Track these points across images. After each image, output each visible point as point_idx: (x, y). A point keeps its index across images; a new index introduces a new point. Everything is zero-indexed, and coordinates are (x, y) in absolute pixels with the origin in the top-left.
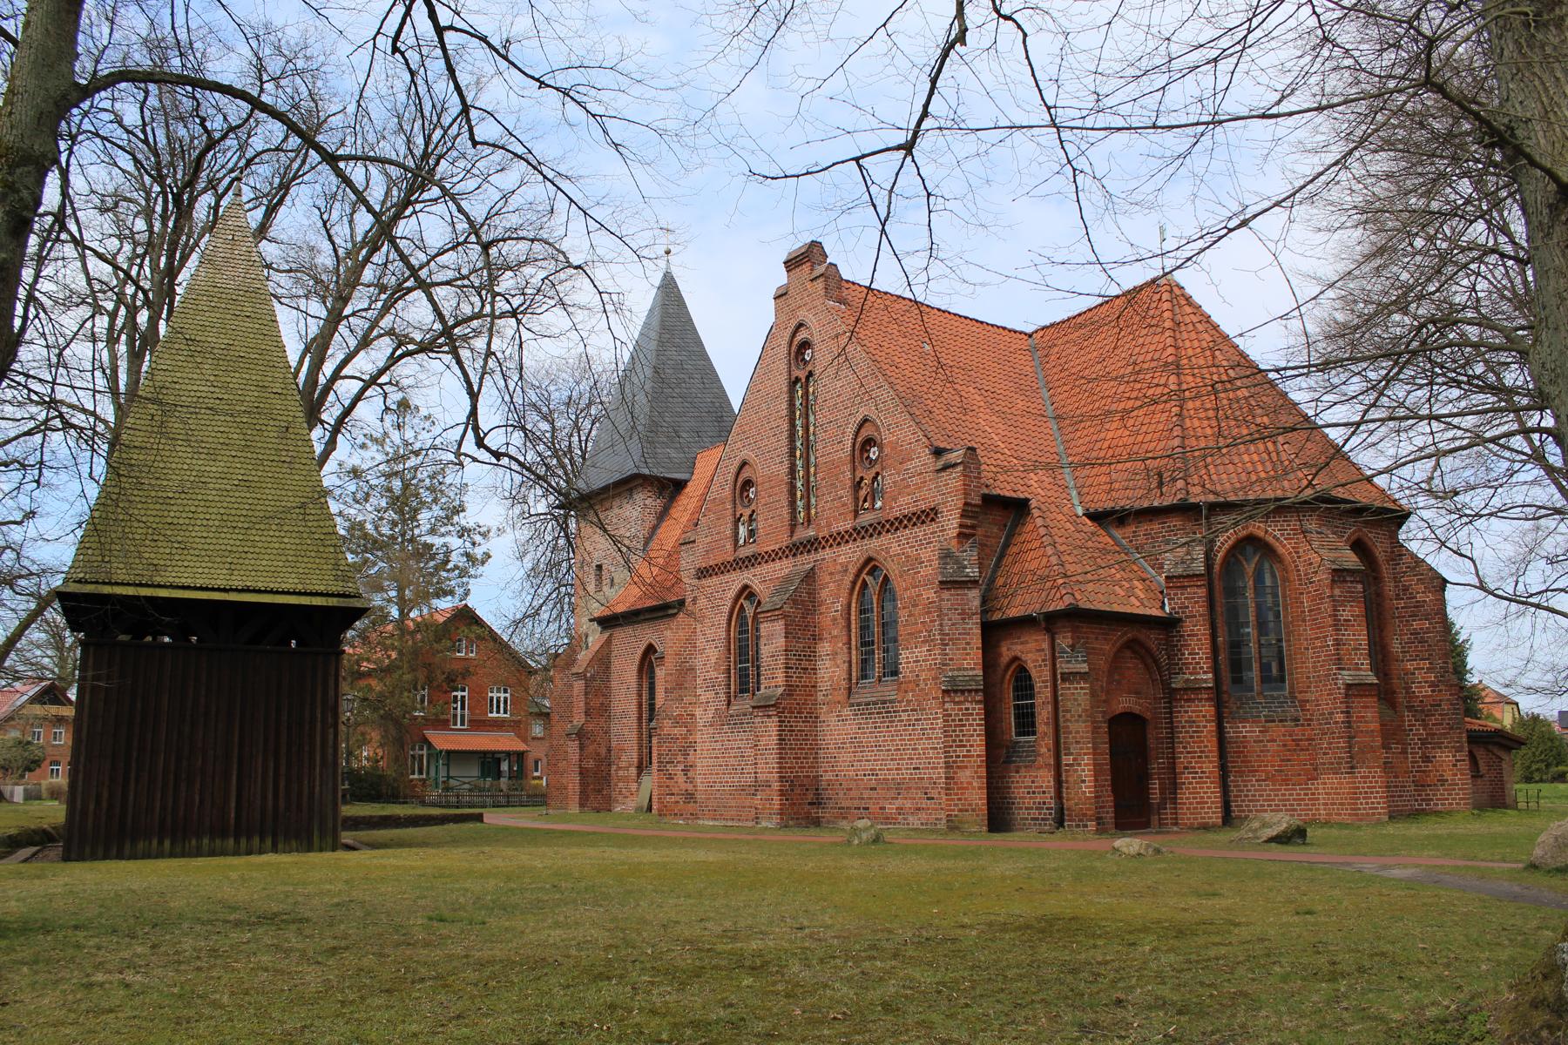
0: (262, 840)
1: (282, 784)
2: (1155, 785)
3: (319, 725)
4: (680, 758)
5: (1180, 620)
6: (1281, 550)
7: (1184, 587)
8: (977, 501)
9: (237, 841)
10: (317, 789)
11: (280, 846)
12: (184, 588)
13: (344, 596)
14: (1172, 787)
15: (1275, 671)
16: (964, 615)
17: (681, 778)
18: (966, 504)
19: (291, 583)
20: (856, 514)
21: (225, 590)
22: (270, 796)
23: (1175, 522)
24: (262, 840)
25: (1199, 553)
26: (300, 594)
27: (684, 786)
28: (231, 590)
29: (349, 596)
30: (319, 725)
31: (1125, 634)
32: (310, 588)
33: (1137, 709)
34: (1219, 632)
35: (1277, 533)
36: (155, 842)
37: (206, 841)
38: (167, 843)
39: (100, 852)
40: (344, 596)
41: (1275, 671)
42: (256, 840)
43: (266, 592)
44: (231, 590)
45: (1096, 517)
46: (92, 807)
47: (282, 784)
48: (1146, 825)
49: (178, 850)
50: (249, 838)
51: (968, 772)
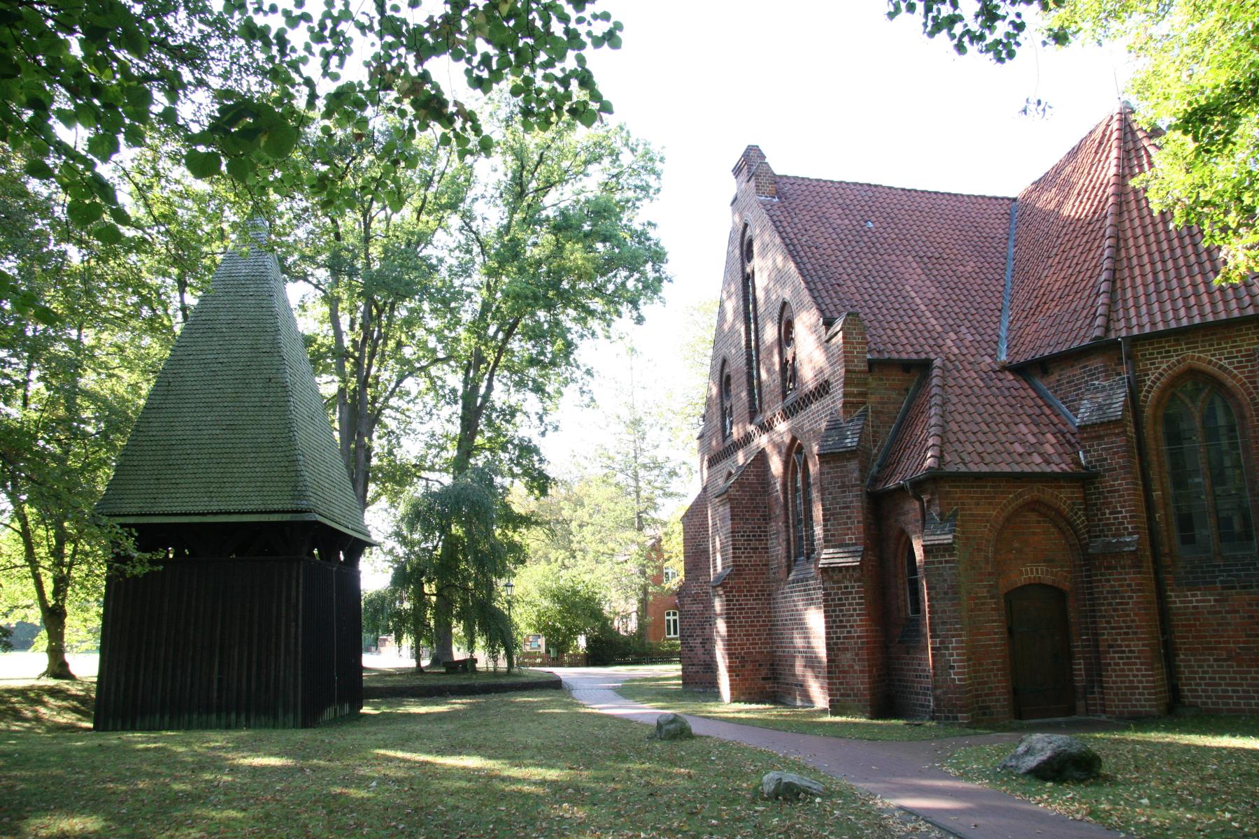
0: (238, 715)
1: (254, 672)
2: (1080, 666)
3: (283, 621)
4: (699, 632)
5: (1097, 475)
6: (1230, 382)
7: (1099, 438)
8: (863, 367)
9: (219, 717)
10: (282, 674)
11: (252, 721)
12: (185, 514)
13: (297, 512)
14: (1097, 669)
15: (1237, 527)
16: (844, 487)
17: (700, 651)
18: (847, 371)
19: (256, 504)
20: (785, 396)
21: (203, 514)
22: (244, 680)
23: (1097, 363)
24: (238, 715)
25: (1120, 398)
26: (261, 512)
27: (702, 657)
28: (208, 513)
29: (301, 512)
30: (283, 621)
31: (1021, 495)
32: (271, 507)
33: (1048, 579)
34: (1156, 485)
35: (1224, 362)
36: (158, 717)
37: (195, 716)
38: (167, 718)
39: (129, 726)
40: (297, 512)
41: (1237, 527)
42: (233, 716)
43: (235, 513)
44: (208, 513)
45: (1023, 370)
46: (113, 688)
47: (254, 672)
48: (1071, 711)
49: (223, 722)
50: (228, 714)
51: (849, 655)
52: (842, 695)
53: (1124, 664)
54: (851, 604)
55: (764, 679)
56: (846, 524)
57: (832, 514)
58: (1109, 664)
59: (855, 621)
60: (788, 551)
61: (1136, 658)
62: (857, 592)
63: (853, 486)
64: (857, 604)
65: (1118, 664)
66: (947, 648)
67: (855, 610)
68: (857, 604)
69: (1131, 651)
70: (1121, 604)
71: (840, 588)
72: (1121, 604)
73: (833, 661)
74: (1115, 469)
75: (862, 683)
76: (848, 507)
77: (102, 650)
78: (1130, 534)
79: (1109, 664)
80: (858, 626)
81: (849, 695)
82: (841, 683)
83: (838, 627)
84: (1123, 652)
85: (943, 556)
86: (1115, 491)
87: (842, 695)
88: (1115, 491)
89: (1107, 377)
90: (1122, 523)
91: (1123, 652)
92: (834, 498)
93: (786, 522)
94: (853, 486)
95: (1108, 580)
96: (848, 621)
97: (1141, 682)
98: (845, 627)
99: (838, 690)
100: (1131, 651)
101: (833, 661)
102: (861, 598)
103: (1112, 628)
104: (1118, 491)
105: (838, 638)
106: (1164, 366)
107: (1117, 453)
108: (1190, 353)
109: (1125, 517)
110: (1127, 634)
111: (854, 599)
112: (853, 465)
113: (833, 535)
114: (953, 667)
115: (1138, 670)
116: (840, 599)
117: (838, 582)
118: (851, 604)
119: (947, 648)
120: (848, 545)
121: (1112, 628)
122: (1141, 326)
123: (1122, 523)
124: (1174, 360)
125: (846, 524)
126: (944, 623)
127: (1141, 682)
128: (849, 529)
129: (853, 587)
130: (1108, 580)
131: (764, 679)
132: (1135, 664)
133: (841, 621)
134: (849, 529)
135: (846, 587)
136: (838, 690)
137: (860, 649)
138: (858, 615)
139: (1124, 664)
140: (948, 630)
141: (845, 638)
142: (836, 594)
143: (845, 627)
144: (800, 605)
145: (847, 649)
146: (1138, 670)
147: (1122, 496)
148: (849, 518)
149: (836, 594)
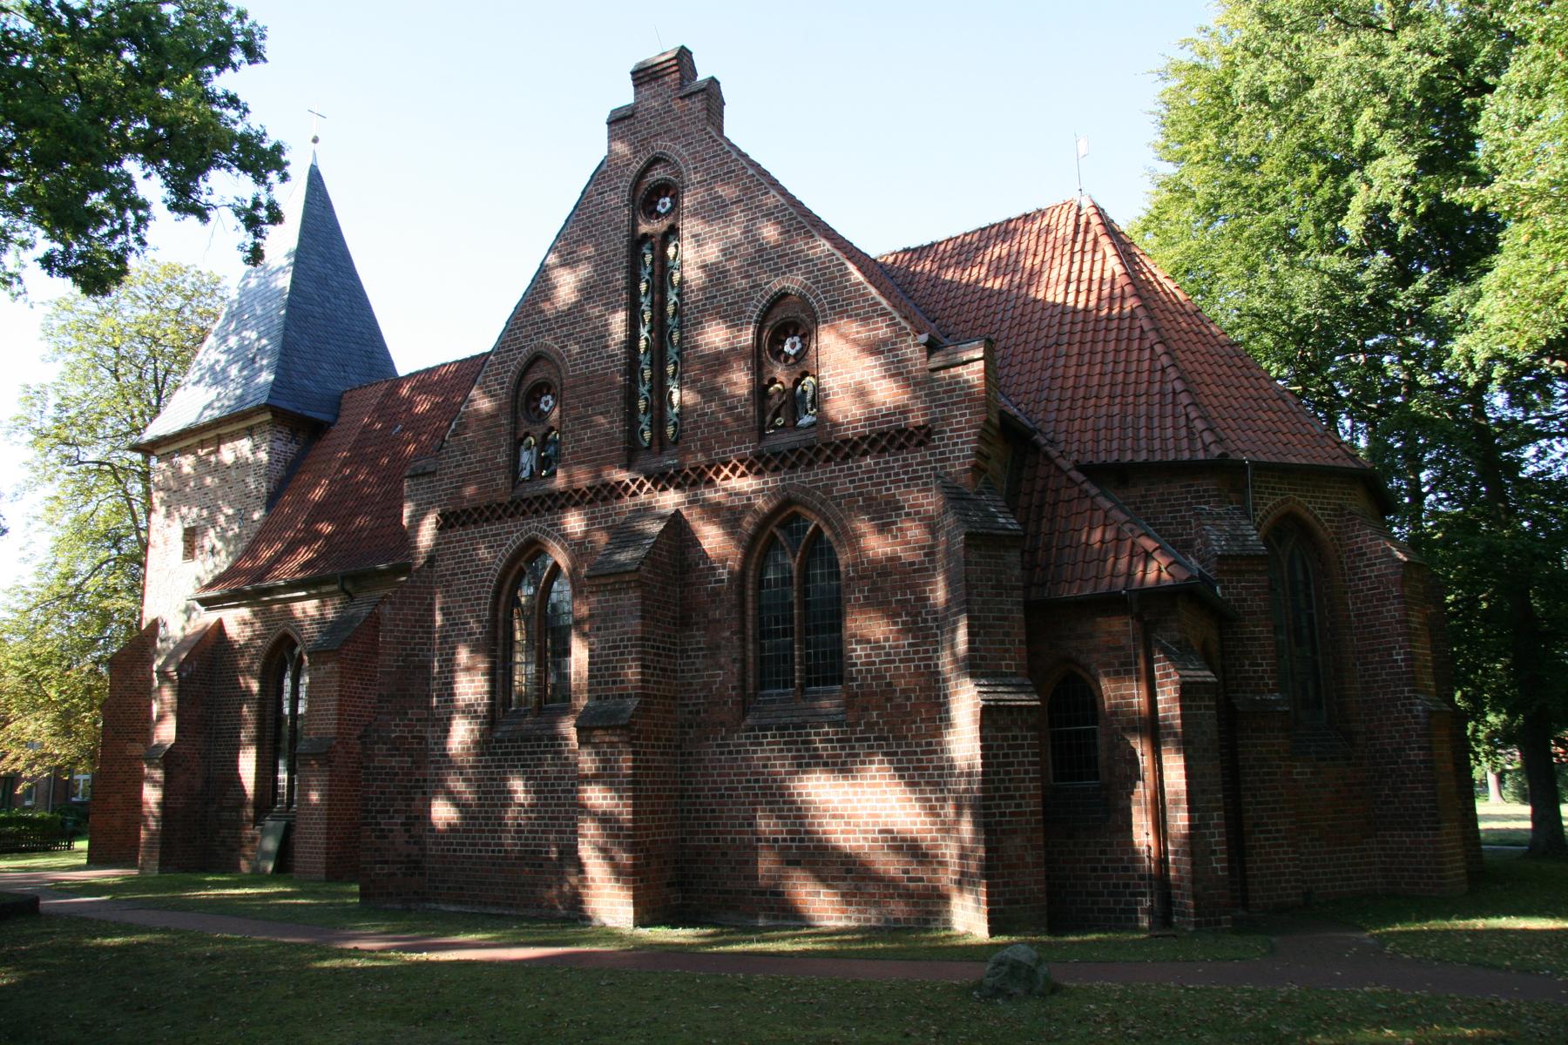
51: (1018, 841)
52: (1008, 902)
53: (1271, 846)
54: (1021, 764)
55: (669, 885)
56: (1002, 642)
57: (981, 627)
58: (1254, 847)
59: (1027, 789)
60: (743, 679)
61: (1284, 838)
62: (1030, 746)
63: (1014, 588)
64: (1031, 763)
65: (1262, 847)
66: (1207, 826)
67: (1027, 772)
68: (1031, 763)
69: (1278, 831)
70: (1269, 774)
71: (1005, 738)
72: (1269, 774)
73: (996, 850)
74: (1255, 613)
75: (1036, 882)
76: (1006, 619)
77: (635, 905)
78: (1271, 692)
79: (1254, 847)
80: (1031, 796)
81: (1017, 902)
82: (1006, 884)
83: (1001, 798)
84: (1269, 832)
85: (1202, 699)
86: (1255, 639)
87: (1008, 902)
88: (1255, 639)
89: (1220, 504)
90: (1262, 678)
91: (1269, 832)
92: (984, 602)
93: (742, 631)
94: (1014, 588)
95: (1255, 746)
96: (1017, 789)
97: (1287, 867)
98: (1013, 797)
99: (1001, 894)
100: (1278, 831)
101: (996, 850)
102: (1034, 755)
103: (1259, 803)
104: (1258, 639)
105: (1003, 814)
106: (1271, 504)
107: (1256, 594)
108: (1291, 494)
109: (1264, 671)
110: (1273, 809)
111: (1025, 755)
112: (1013, 557)
113: (983, 658)
114: (1214, 852)
115: (1285, 853)
116: (1006, 756)
117: (1004, 730)
118: (1021, 764)
119: (1207, 826)
120: (1004, 675)
121: (1259, 803)
122: (1151, 451)
123: (1262, 678)
124: (1279, 498)
125: (1002, 642)
126: (1203, 792)
127: (1287, 867)
128: (1006, 651)
129: (1024, 738)
130: (1255, 746)
131: (669, 885)
132: (1281, 845)
133: (1007, 789)
134: (1006, 651)
135: (1015, 738)
136: (1001, 894)
137: (1033, 830)
138: (1031, 780)
139: (1271, 846)
140: (1209, 801)
141: (1012, 814)
142: (1000, 747)
143: (1013, 797)
144: (780, 767)
145: (1015, 831)
146: (1285, 853)
147: (1262, 645)
148: (1007, 634)
149: (1000, 747)
